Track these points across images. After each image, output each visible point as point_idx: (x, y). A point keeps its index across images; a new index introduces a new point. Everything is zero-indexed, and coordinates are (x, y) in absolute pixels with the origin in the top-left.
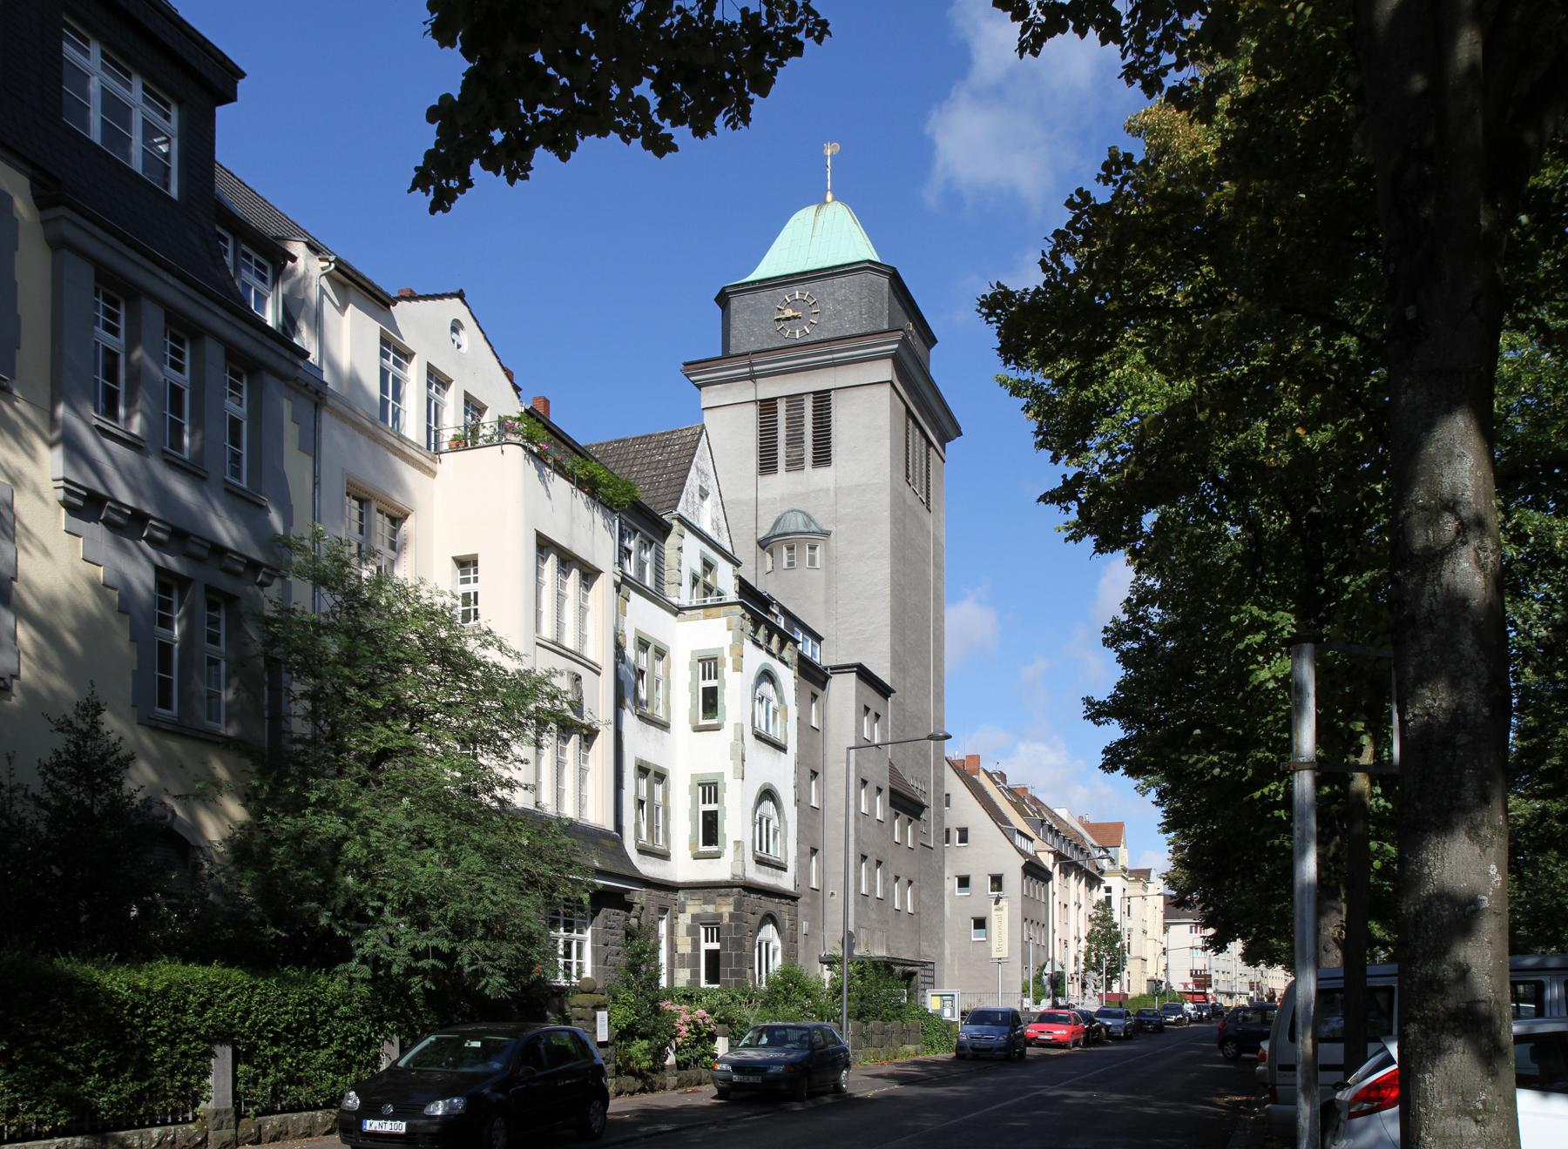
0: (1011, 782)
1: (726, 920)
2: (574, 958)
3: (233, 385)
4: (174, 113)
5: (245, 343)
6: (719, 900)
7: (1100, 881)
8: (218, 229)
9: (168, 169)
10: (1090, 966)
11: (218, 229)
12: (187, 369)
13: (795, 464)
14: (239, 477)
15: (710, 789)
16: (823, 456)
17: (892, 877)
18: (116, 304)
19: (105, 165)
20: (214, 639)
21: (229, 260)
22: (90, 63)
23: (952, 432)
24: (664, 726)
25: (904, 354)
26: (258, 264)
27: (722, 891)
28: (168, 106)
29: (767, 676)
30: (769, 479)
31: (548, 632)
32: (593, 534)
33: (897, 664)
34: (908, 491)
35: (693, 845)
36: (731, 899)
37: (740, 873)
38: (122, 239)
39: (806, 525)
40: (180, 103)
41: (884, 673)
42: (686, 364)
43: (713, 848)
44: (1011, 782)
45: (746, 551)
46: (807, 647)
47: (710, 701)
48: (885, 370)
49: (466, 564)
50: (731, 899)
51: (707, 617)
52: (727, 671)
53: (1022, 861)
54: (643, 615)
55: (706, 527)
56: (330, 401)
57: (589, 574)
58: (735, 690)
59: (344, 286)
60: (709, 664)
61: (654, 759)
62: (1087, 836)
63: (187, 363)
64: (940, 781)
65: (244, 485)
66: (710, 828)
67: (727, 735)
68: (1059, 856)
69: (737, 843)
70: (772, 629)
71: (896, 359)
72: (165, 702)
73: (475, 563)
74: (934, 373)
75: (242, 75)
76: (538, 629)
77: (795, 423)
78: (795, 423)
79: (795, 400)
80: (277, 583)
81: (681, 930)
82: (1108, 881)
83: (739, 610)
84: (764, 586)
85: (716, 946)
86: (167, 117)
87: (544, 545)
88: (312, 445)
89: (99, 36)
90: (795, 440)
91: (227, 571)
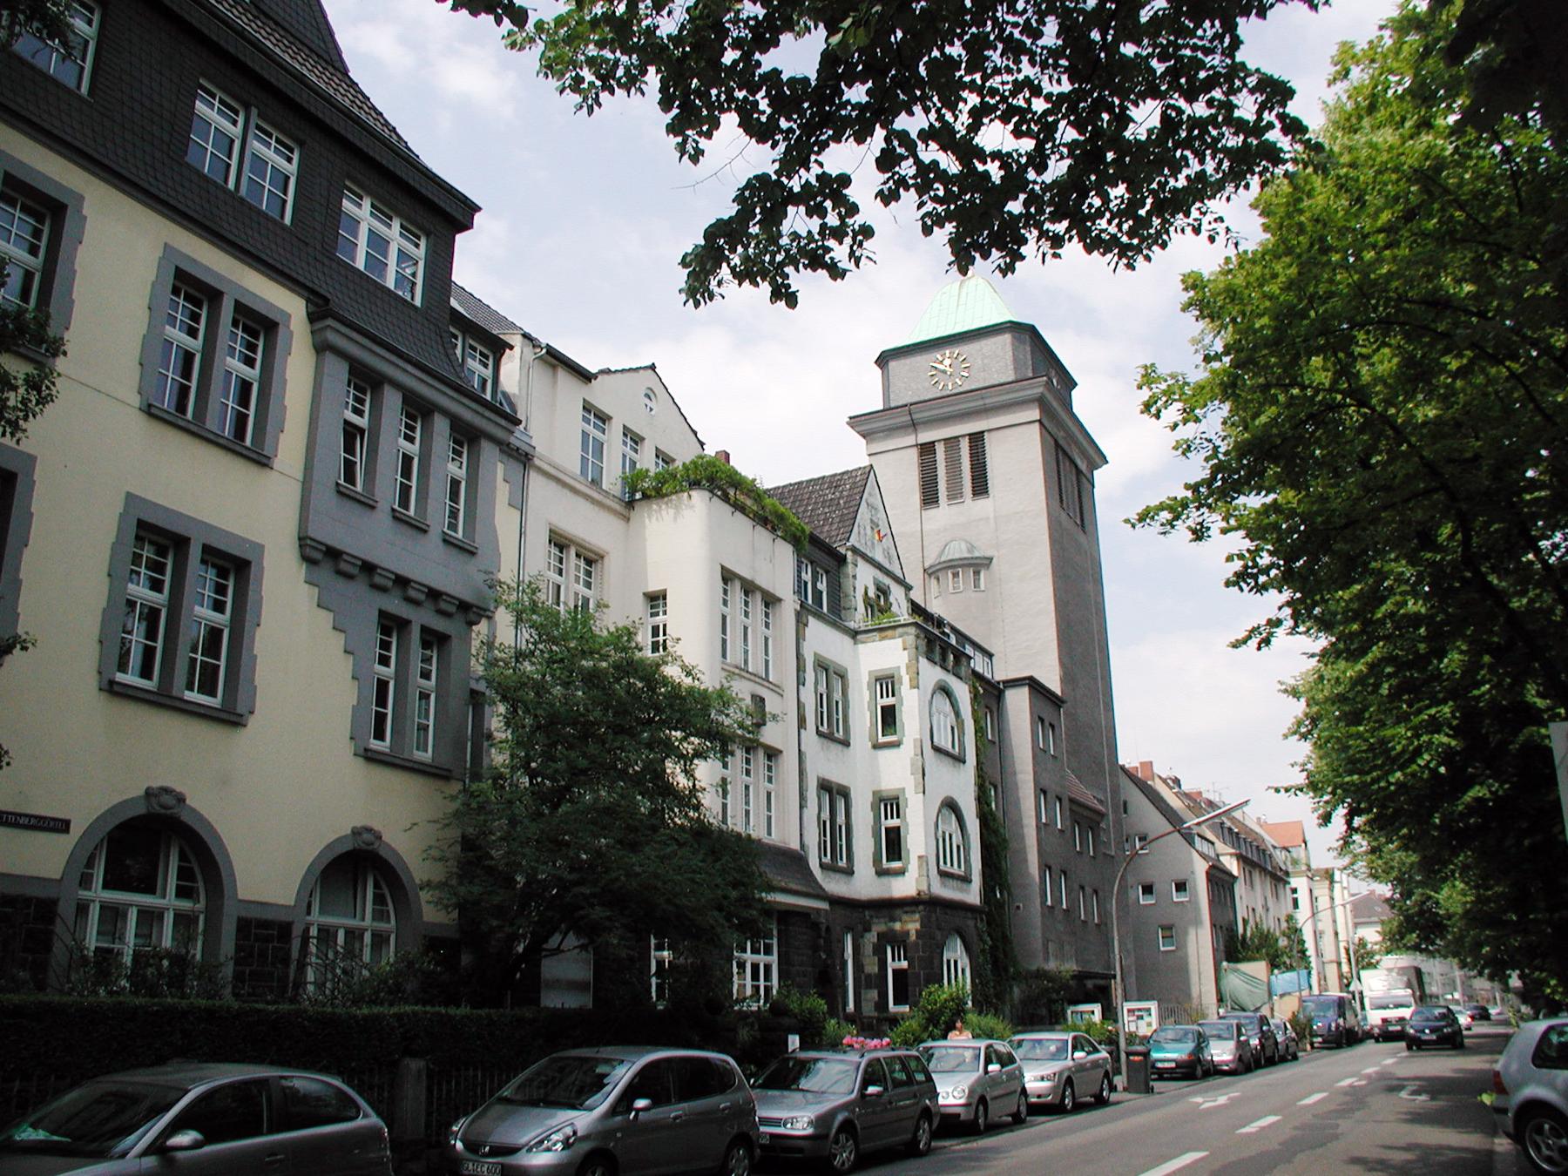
0: (1186, 787)
2: (762, 983)
3: (455, 451)
4: (423, 243)
5: (467, 415)
6: (905, 917)
8: (452, 329)
9: (229, 165)
10: (1387, 488)
11: (452, 329)
12: (367, 414)
13: (955, 494)
14: (407, 508)
15: (889, 803)
16: (981, 487)
17: (1076, 887)
18: (199, 305)
19: (367, 286)
20: (426, 675)
21: (459, 352)
22: (361, 211)
23: (1098, 461)
24: (846, 743)
25: (1049, 397)
26: (481, 354)
28: (292, 151)
29: (945, 690)
30: (932, 513)
31: (735, 656)
32: (776, 566)
33: (1067, 677)
34: (1064, 515)
35: (877, 861)
36: (917, 916)
37: (924, 888)
38: (400, 355)
39: (969, 551)
40: (428, 235)
41: (1054, 683)
43: (896, 865)
44: (1186, 787)
45: (914, 577)
46: (979, 663)
47: (889, 717)
48: (1035, 414)
49: (656, 600)
50: (917, 916)
51: (883, 639)
52: (905, 689)
54: (822, 639)
55: (879, 557)
56: (537, 462)
57: (771, 601)
58: (911, 706)
59: (554, 367)
60: (886, 682)
61: (836, 777)
63: (418, 435)
64: (1116, 790)
65: (460, 535)
66: (894, 844)
67: (908, 750)
68: (1241, 858)
69: (920, 857)
70: (945, 648)
71: (1041, 402)
72: (379, 735)
73: (665, 598)
74: (1077, 409)
75: (479, 209)
76: (724, 656)
79: (952, 442)
80: (484, 622)
81: (868, 949)
82: (1294, 882)
83: (912, 630)
84: (935, 608)
85: (904, 964)
86: (417, 246)
87: (728, 576)
88: (519, 503)
89: (370, 193)
91: (409, 600)
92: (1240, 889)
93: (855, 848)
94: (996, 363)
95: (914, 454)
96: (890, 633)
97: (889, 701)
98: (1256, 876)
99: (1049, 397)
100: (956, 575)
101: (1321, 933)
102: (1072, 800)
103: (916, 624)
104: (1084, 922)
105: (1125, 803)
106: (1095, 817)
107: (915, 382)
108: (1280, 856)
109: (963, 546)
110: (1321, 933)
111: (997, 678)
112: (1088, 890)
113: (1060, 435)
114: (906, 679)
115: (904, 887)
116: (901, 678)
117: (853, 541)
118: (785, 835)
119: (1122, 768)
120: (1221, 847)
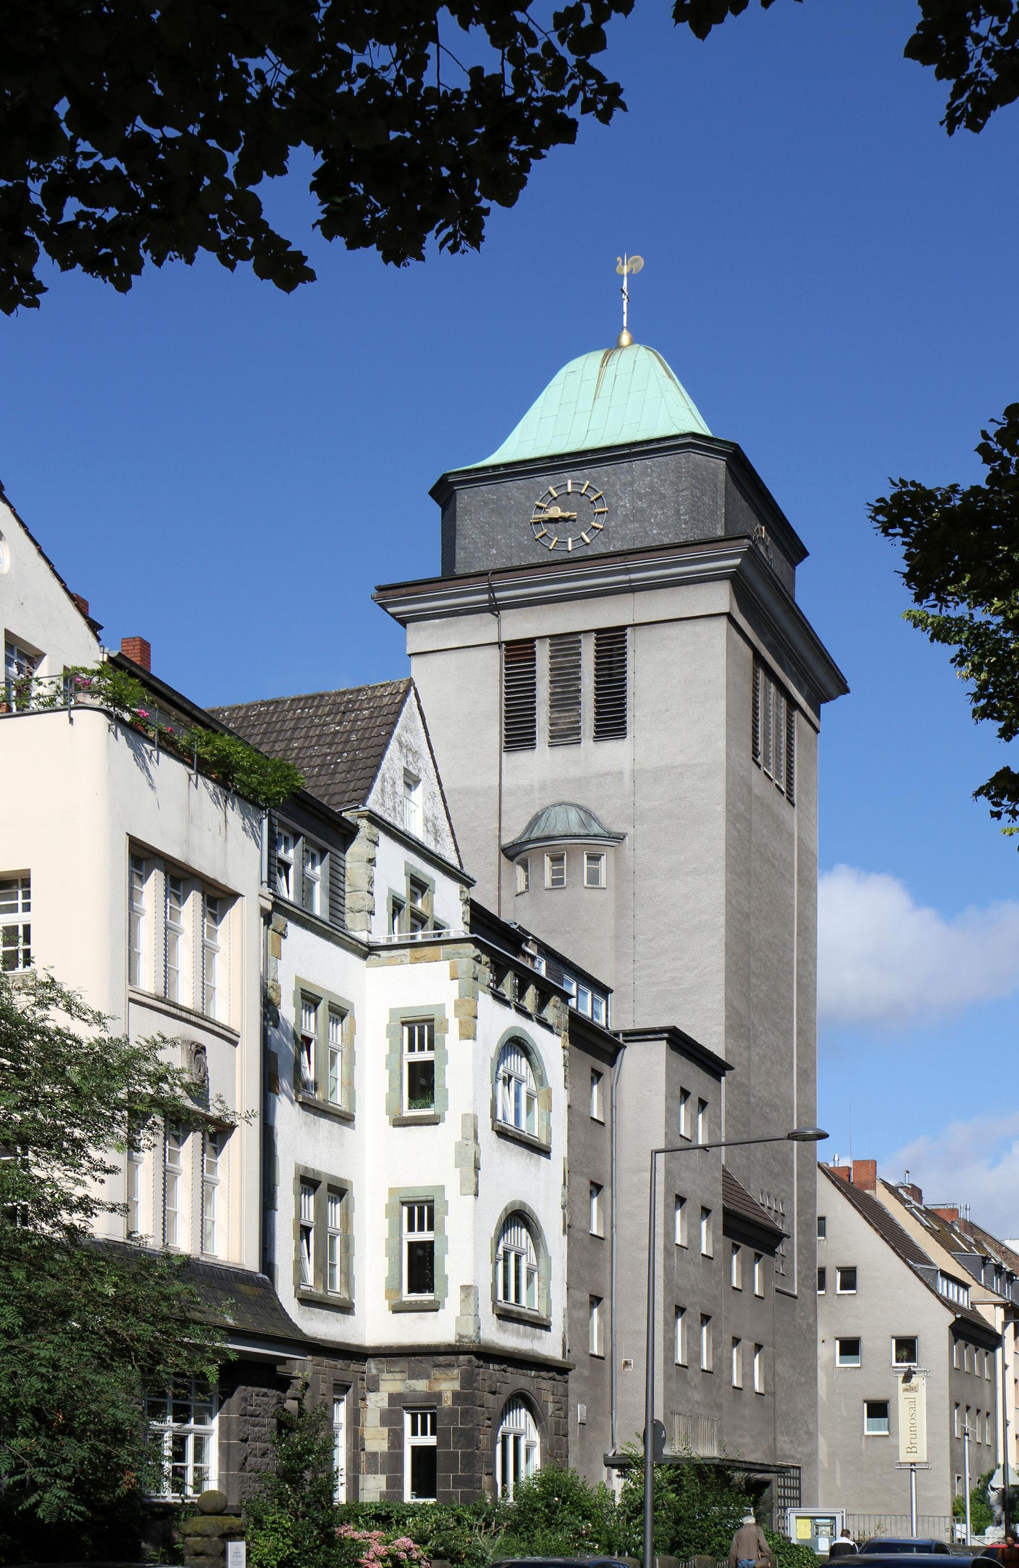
0: (930, 1200)
1: (447, 1402)
6: (435, 1373)
13: (565, 735)
15: (421, 1211)
16: (612, 723)
17: (727, 1338)
23: (831, 688)
30: (522, 757)
31: (148, 982)
33: (737, 1025)
34: (756, 776)
35: (392, 1290)
36: (456, 1372)
37: (470, 1331)
39: (583, 824)
42: (380, 589)
43: (426, 1297)
44: (930, 1200)
47: (422, 1082)
48: (719, 597)
51: (416, 960)
52: (451, 1039)
53: (950, 1318)
54: (308, 958)
55: (417, 830)
57: (218, 899)
58: (464, 1070)
60: (421, 1030)
61: (325, 1163)
64: (809, 1198)
66: (422, 1268)
67: (449, 1132)
70: (526, 978)
71: (737, 581)
79: (565, 644)
83: (470, 950)
84: (512, 914)
87: (142, 857)
90: (565, 699)
93: (356, 1271)
95: (493, 660)
103: (476, 942)
105: (822, 1219)
111: (613, 1027)
112: (747, 1344)
114: (454, 1025)
115: (438, 1329)
116: (445, 1022)
117: (373, 803)
118: (233, 1246)
120: (977, 1291)
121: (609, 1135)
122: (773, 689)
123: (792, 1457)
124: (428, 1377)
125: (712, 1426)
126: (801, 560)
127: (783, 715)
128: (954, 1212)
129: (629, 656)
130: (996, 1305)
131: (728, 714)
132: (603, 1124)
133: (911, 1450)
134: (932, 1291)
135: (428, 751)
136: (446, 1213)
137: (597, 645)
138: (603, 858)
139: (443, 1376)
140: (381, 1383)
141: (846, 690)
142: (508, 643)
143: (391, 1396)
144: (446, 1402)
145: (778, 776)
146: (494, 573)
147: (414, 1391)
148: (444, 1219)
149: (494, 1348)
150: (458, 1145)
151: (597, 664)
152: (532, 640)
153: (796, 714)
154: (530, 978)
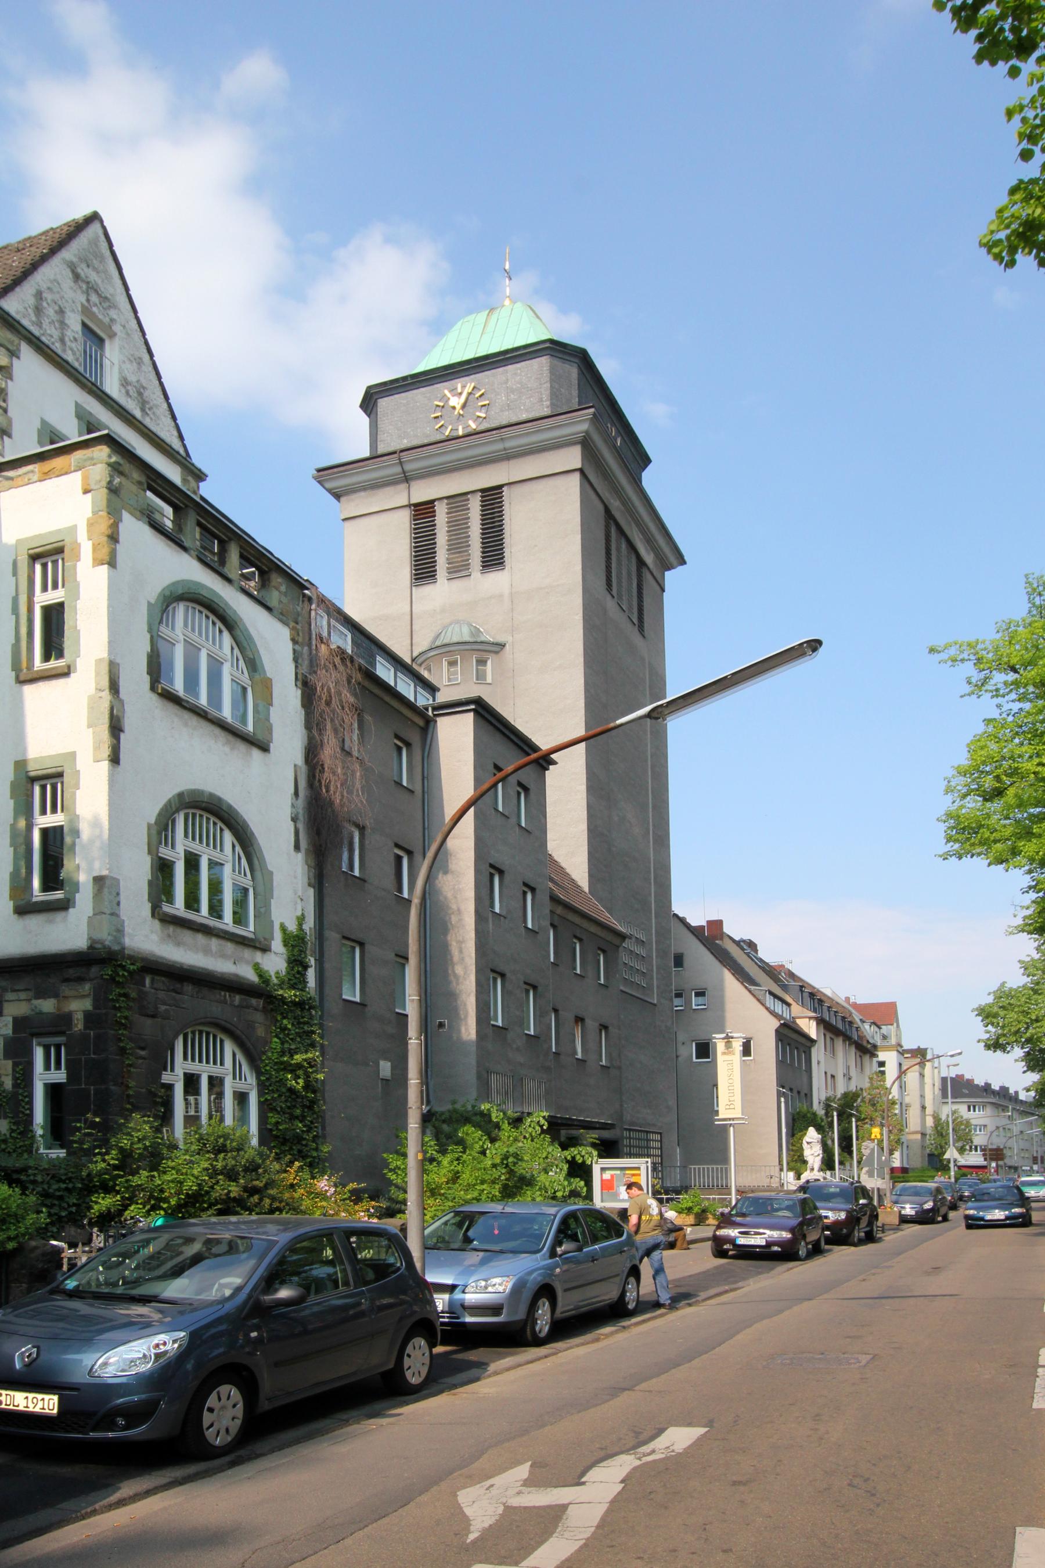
1: (79, 1025)
6: (66, 990)
7: (873, 1055)
13: (459, 570)
16: (494, 556)
23: (672, 559)
25: (596, 438)
27: (71, 972)
30: (427, 591)
34: (611, 604)
36: (87, 987)
37: (105, 935)
39: (472, 634)
42: (319, 471)
43: (59, 895)
48: (573, 457)
51: (46, 476)
53: (775, 1024)
62: (853, 1011)
68: (821, 1022)
71: (586, 444)
77: (458, 528)
78: (458, 528)
79: (457, 501)
82: (882, 1056)
90: (459, 545)
92: (818, 1053)
94: (527, 391)
95: (404, 518)
96: (58, 462)
97: (53, 597)
98: (839, 1043)
99: (596, 438)
100: (452, 664)
101: (908, 1106)
102: (554, 899)
104: (582, 1062)
106: (610, 937)
107: (409, 422)
108: (868, 1029)
109: (465, 630)
110: (908, 1106)
112: (591, 1024)
113: (615, 505)
115: (69, 933)
119: (675, 915)
120: (796, 1009)
121: (420, 803)
122: (624, 545)
123: (654, 1125)
124: (56, 995)
125: (539, 1087)
126: (646, 466)
127: (634, 569)
128: (783, 966)
129: (506, 503)
130: (810, 1018)
131: (667, 768)
132: (412, 792)
133: (730, 1107)
134: (763, 1005)
135: (129, 307)
136: (77, 786)
137: (482, 501)
138: (489, 663)
139: (72, 993)
140: (6, 1005)
141: (683, 562)
142: (416, 505)
143: (16, 1021)
144: (76, 1025)
145: (630, 607)
146: (402, 451)
147: (41, 1013)
148: (75, 794)
149: (162, 964)
150: (91, 698)
151: (482, 515)
152: (432, 502)
153: (644, 570)
154: (230, 539)
